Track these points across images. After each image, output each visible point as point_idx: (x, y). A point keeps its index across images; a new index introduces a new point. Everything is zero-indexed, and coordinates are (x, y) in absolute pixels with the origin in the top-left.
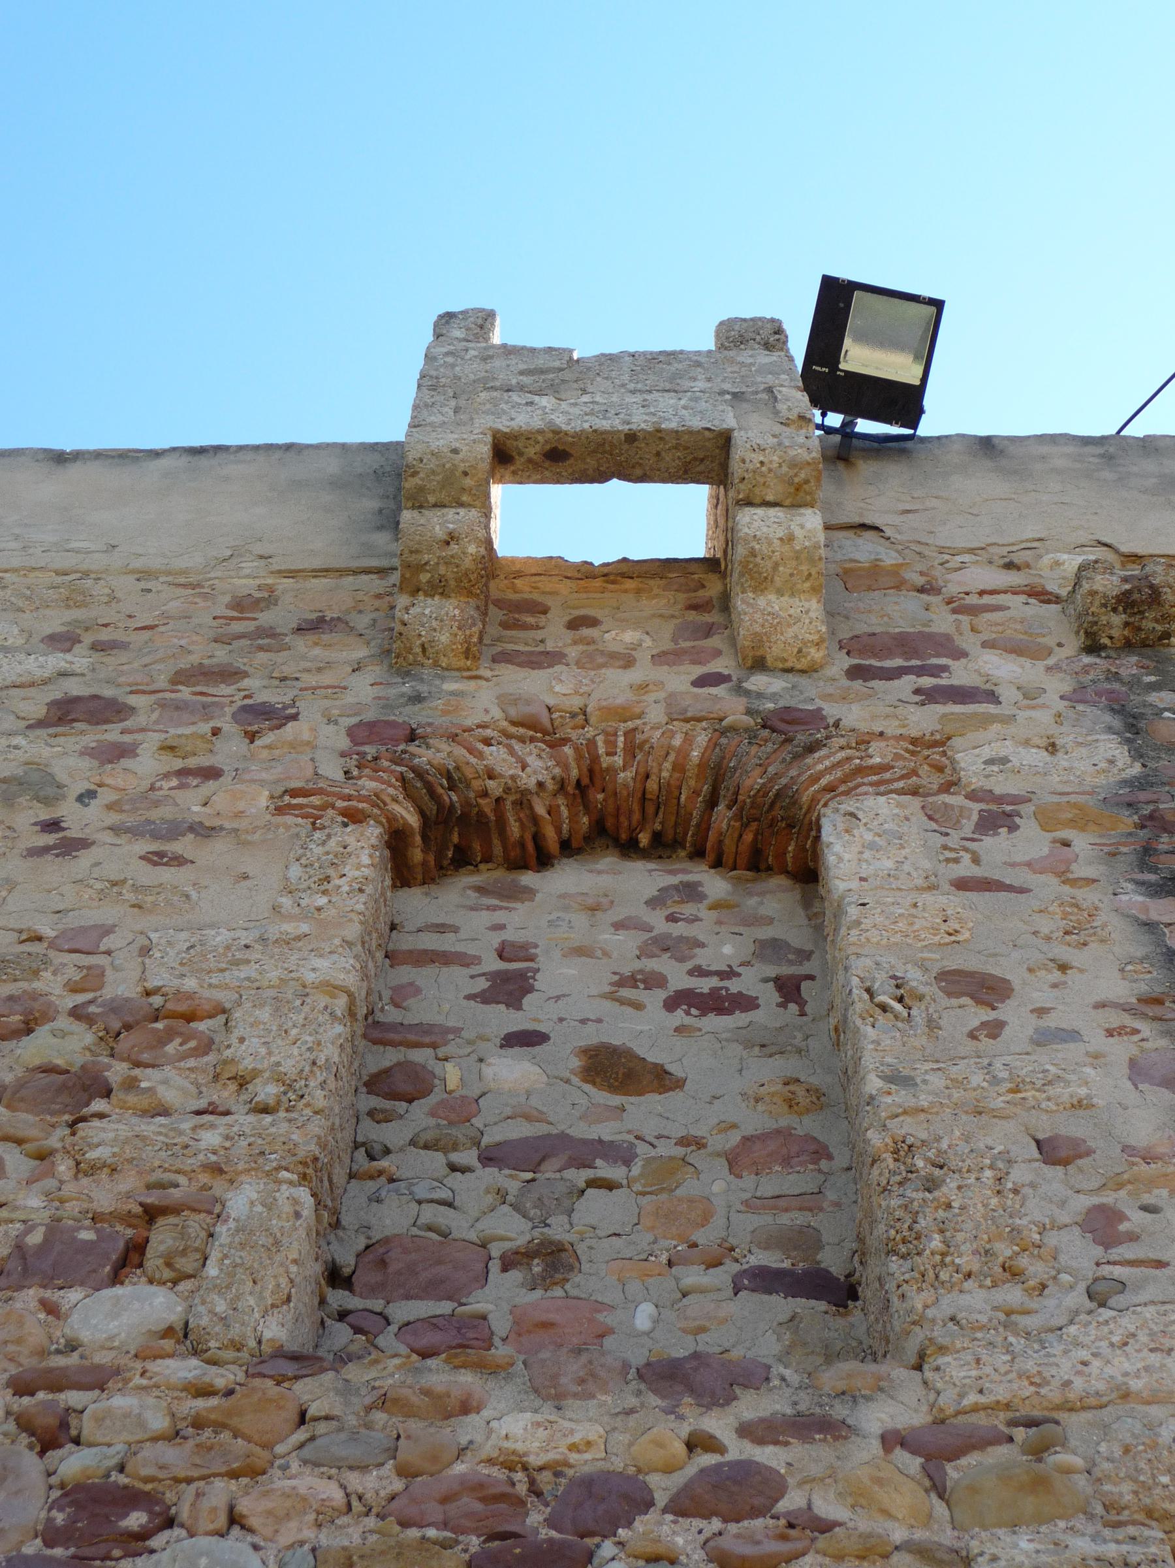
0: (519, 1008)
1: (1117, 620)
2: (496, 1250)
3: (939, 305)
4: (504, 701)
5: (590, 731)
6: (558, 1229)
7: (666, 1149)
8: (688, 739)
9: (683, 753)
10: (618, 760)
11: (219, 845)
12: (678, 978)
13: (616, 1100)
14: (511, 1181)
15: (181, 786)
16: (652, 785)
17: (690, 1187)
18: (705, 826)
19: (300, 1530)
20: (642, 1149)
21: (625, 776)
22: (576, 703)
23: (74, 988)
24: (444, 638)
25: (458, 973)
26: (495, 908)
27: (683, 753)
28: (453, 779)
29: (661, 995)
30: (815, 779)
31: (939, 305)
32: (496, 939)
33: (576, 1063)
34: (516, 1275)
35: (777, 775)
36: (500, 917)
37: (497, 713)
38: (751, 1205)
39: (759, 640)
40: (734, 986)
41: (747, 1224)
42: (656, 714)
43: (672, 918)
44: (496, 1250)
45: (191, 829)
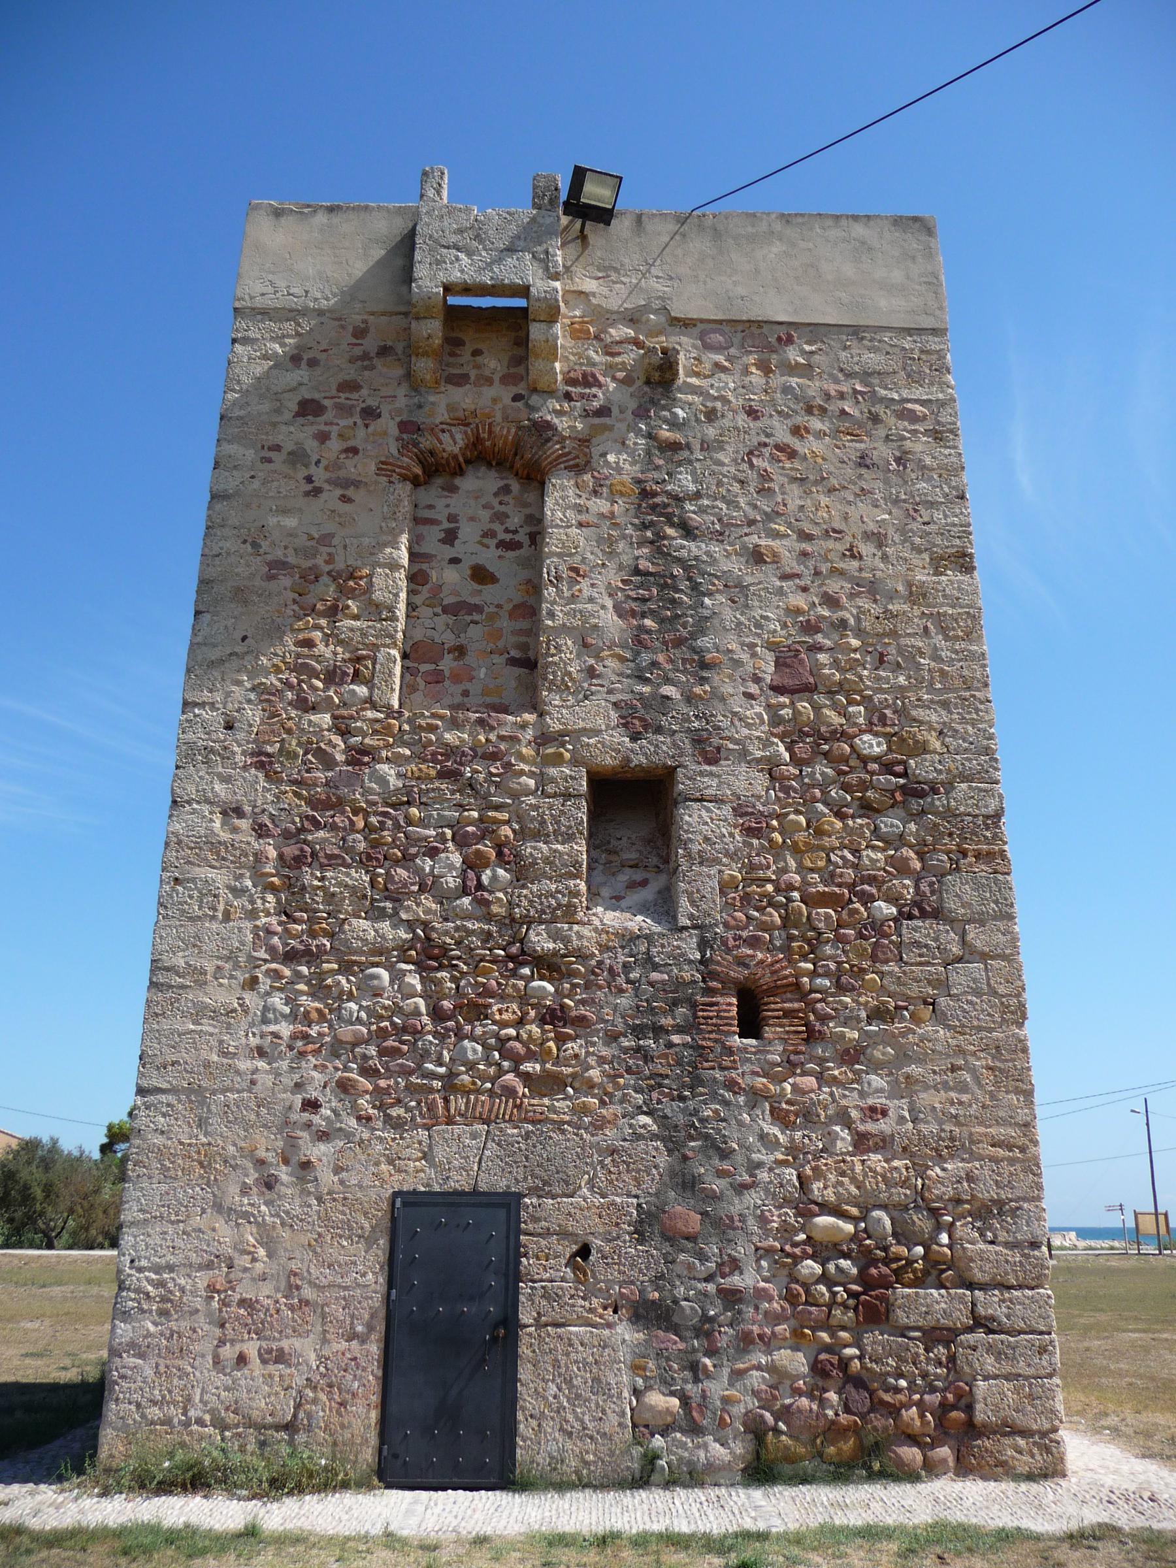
0: (452, 545)
1: (657, 374)
2: (446, 646)
3: (621, 178)
4: (451, 408)
5: (477, 421)
6: (462, 640)
7: (492, 609)
8: (509, 431)
9: (506, 437)
10: (486, 436)
11: (362, 492)
12: (502, 536)
13: (480, 587)
14: (450, 619)
15: (347, 458)
16: (496, 449)
17: (498, 624)
18: (513, 462)
19: (394, 566)
20: (486, 608)
21: (488, 443)
22: (473, 407)
23: (327, 562)
24: (428, 377)
25: (436, 528)
26: (447, 497)
27: (506, 437)
28: (432, 453)
29: (495, 541)
30: (546, 459)
31: (621, 178)
32: (446, 512)
33: (469, 572)
34: (451, 656)
35: (536, 453)
36: (448, 501)
37: (446, 416)
38: (515, 633)
39: (535, 382)
40: (517, 537)
41: (513, 639)
42: (498, 417)
43: (501, 503)
44: (446, 646)
45: (352, 483)
